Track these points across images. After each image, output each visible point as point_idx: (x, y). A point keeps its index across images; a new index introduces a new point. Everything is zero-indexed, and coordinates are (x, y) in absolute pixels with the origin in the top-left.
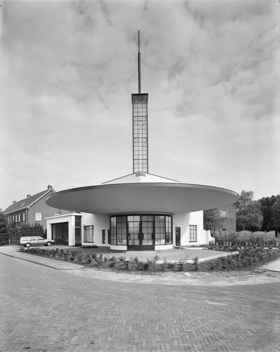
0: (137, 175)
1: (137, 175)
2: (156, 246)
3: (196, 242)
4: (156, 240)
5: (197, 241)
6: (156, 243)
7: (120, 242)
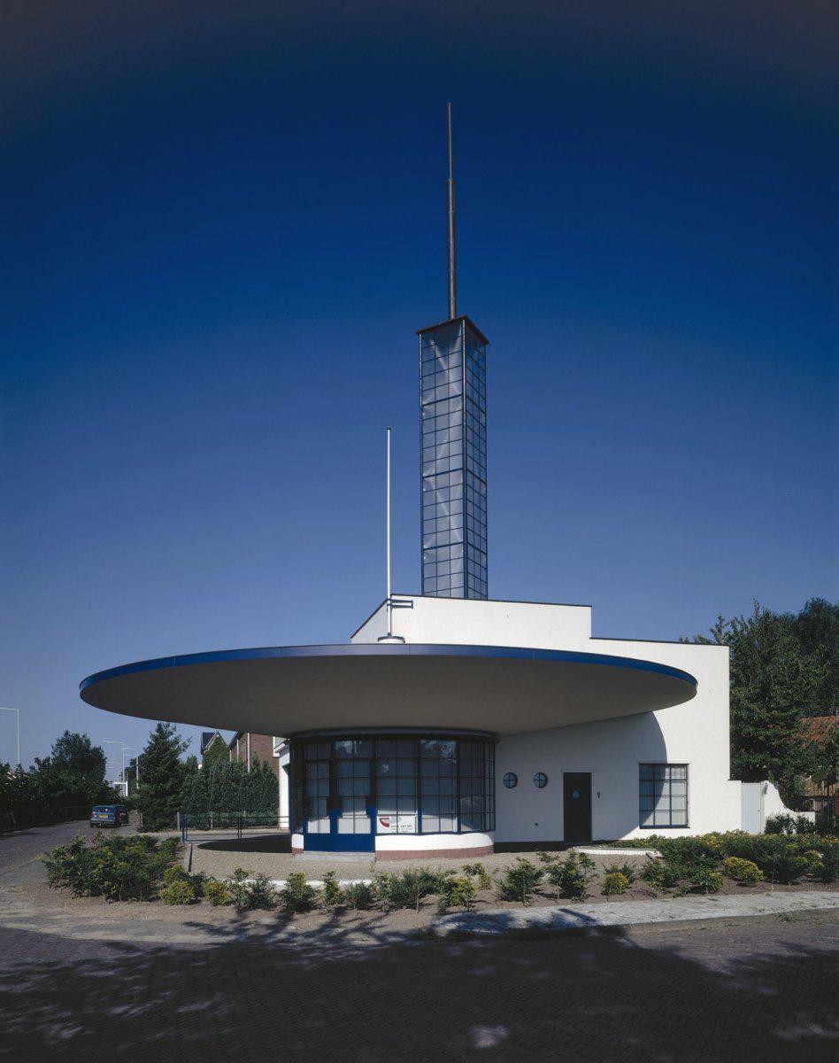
0: (410, 604)
1: (410, 604)
2: (377, 839)
3: (685, 826)
4: (378, 818)
5: (691, 824)
6: (380, 828)
7: (387, 825)
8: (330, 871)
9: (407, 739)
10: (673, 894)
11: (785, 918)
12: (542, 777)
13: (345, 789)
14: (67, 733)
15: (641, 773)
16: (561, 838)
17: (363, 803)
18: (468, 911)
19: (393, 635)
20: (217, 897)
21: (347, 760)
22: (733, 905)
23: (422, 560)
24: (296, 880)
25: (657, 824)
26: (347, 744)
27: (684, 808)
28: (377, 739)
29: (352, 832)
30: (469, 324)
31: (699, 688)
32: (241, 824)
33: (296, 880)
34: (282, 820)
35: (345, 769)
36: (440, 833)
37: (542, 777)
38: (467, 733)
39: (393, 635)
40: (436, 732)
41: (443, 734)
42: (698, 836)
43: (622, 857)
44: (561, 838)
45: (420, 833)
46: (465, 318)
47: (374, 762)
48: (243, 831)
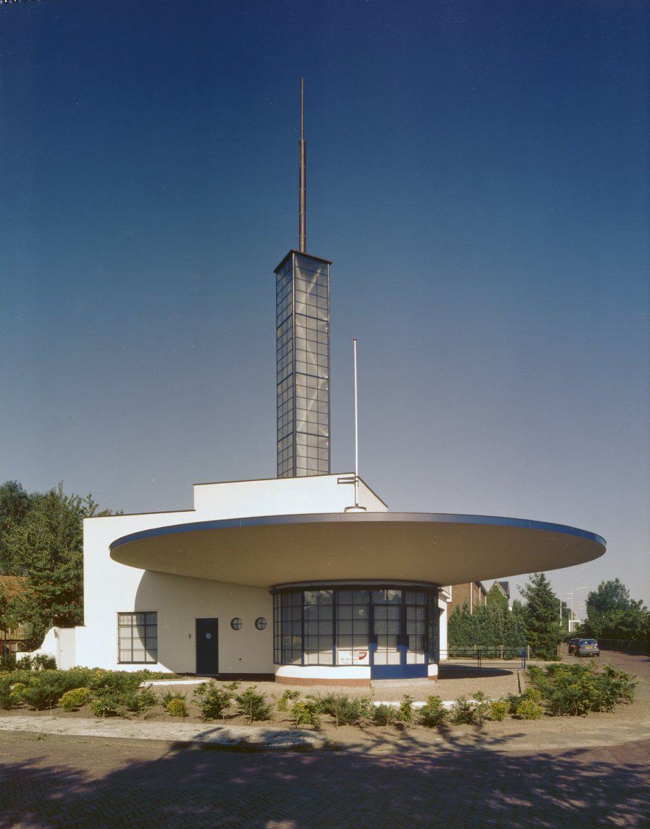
0: (340, 481)
1: (340, 481)
8: (407, 694)
9: (369, 589)
10: (162, 717)
11: (41, 737)
12: (260, 626)
13: (379, 628)
14: (617, 581)
15: (83, 623)
16: (194, 672)
17: (392, 640)
18: (296, 728)
19: (359, 505)
20: (32, 686)
21: (381, 605)
22: (84, 727)
23: (329, 442)
24: (434, 701)
25: (134, 660)
26: (392, 593)
27: (122, 653)
28: (342, 589)
29: (385, 664)
30: (298, 254)
31: (108, 552)
32: (478, 656)
33: (434, 701)
34: (441, 652)
35: (379, 613)
36: (318, 665)
37: (260, 626)
38: (411, 584)
39: (359, 505)
40: (325, 584)
41: (315, 586)
42: (111, 671)
43: (172, 686)
44: (194, 672)
45: (334, 665)
46: (292, 252)
47: (335, 606)
48: (483, 661)
